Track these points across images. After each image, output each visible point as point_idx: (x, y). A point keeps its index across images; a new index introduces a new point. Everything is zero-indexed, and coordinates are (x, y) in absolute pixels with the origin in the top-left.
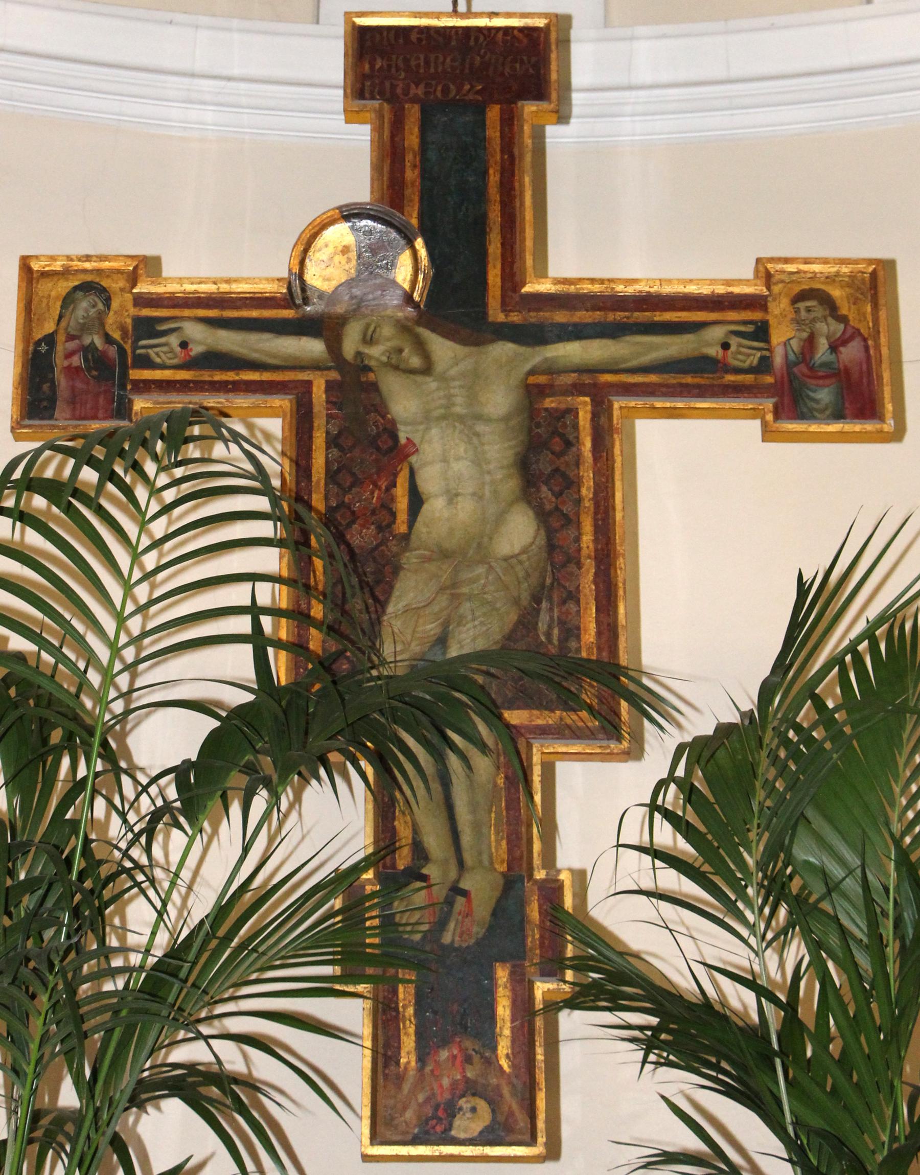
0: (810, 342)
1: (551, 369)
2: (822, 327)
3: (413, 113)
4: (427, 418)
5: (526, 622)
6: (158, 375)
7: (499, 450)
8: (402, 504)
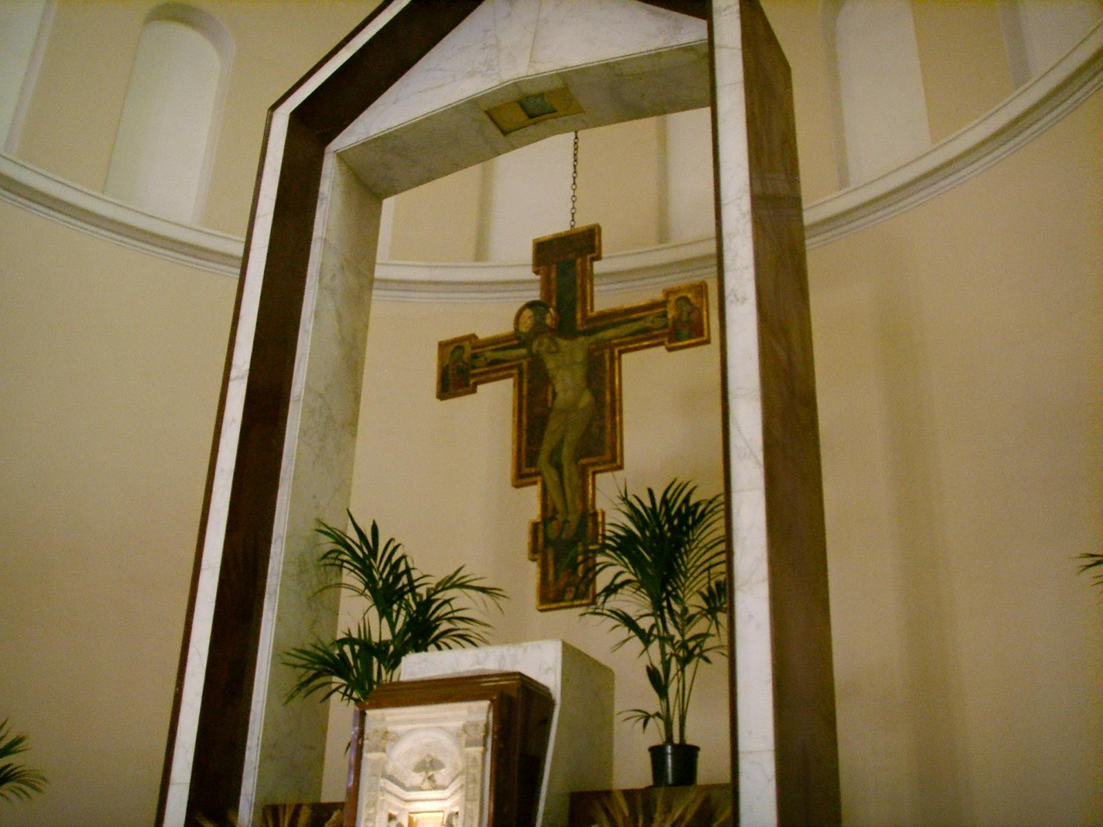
0: (681, 314)
2: (684, 309)
7: (580, 373)
8: (550, 398)
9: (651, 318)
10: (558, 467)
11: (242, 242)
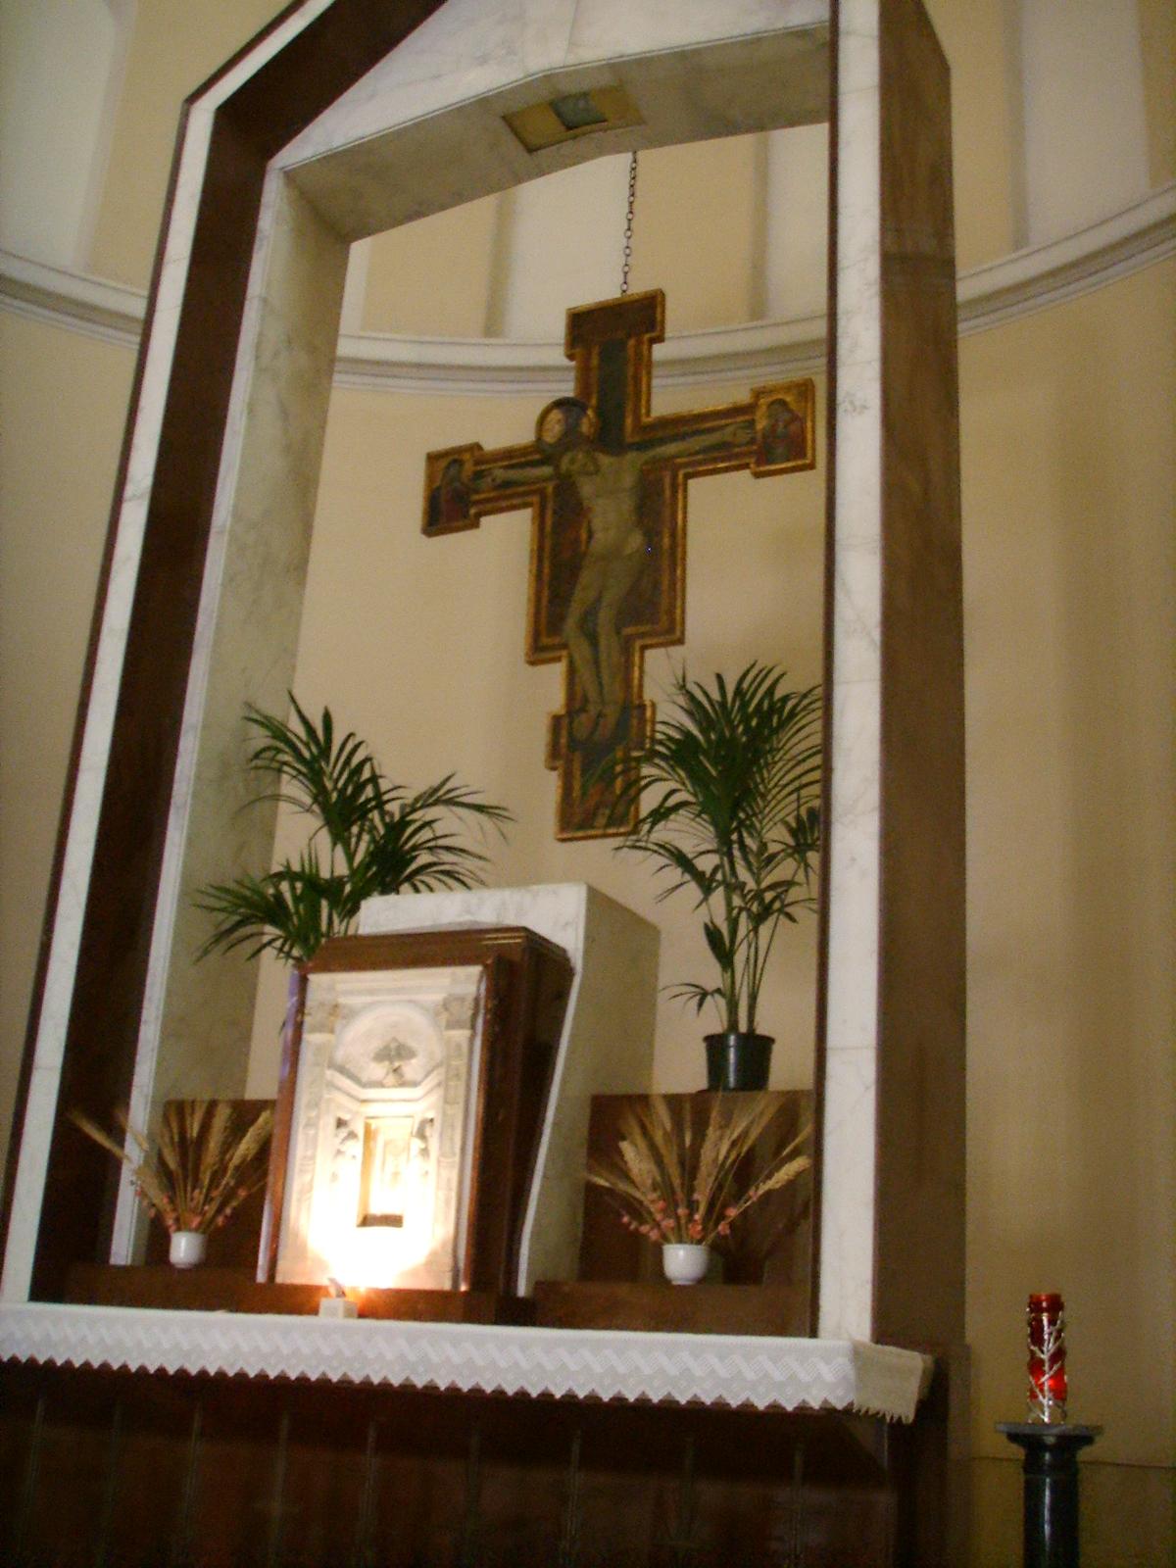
3: (596, 351)
6: (483, 496)
7: (627, 504)
8: (584, 536)
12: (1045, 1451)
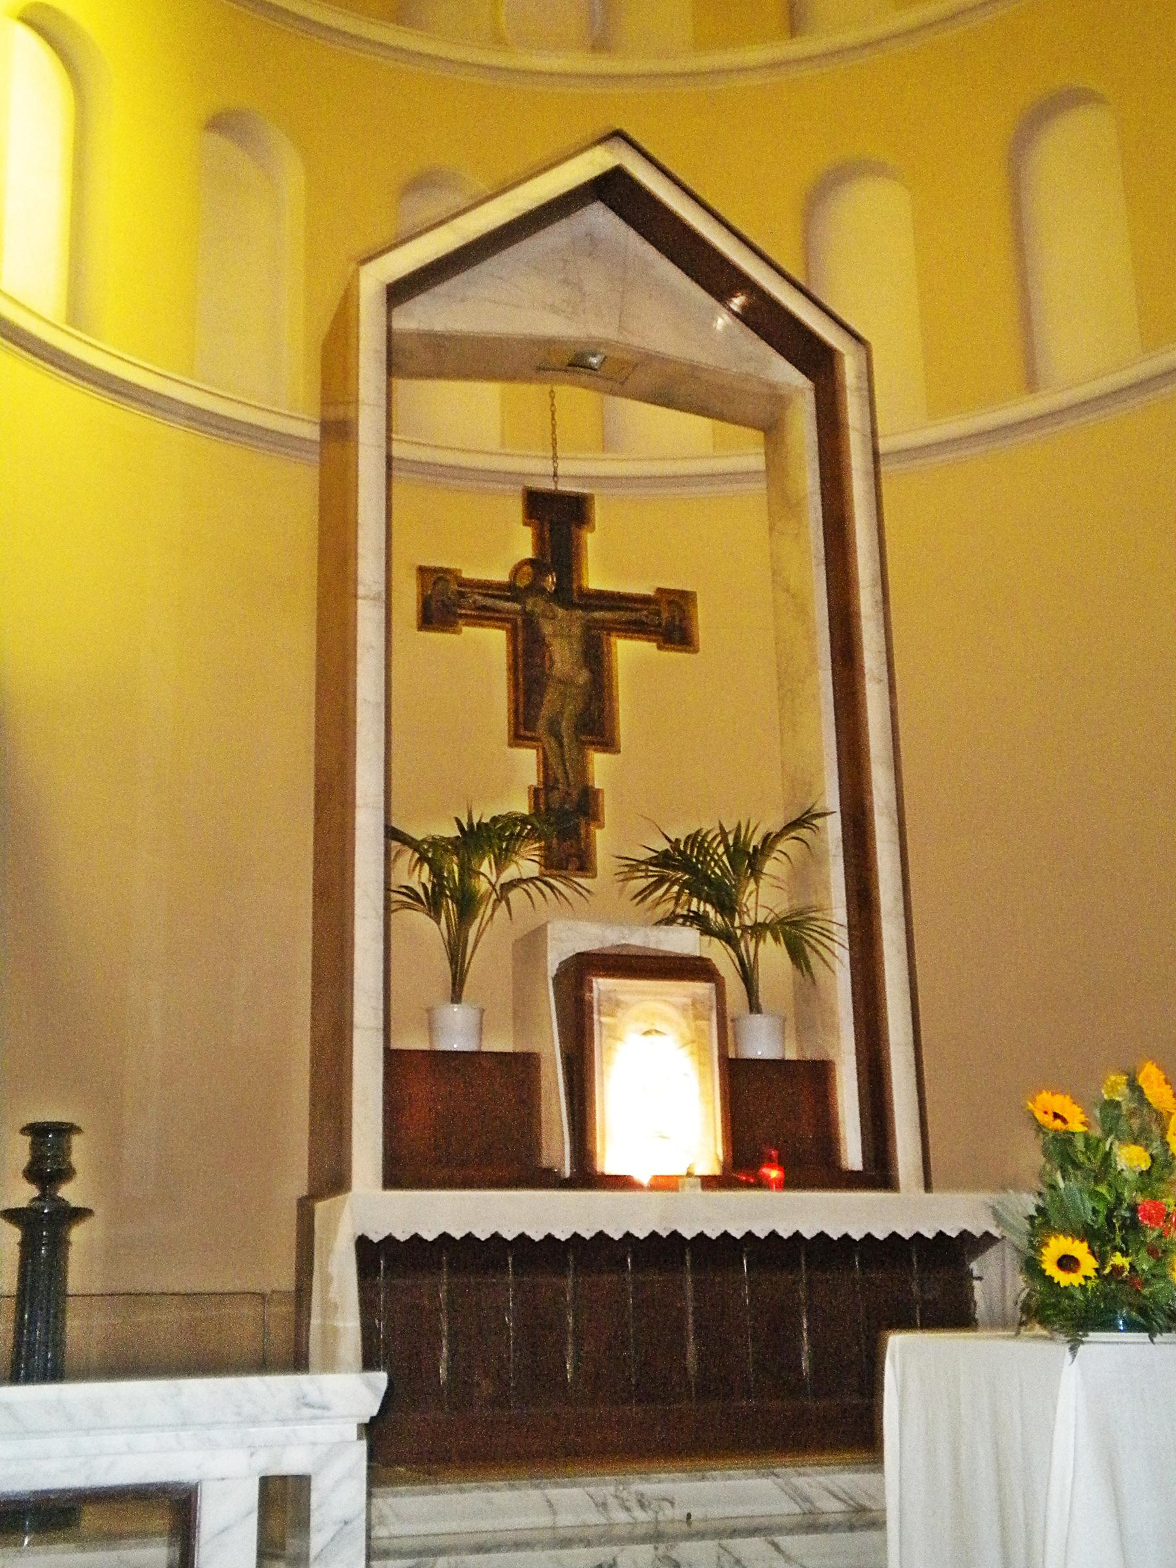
0: (673, 618)
1: (596, 620)
3: (547, 527)
4: (555, 635)
5: (587, 708)
6: (463, 612)
9: (645, 613)
10: (558, 738)
11: (316, 423)
12: (570, 1179)
